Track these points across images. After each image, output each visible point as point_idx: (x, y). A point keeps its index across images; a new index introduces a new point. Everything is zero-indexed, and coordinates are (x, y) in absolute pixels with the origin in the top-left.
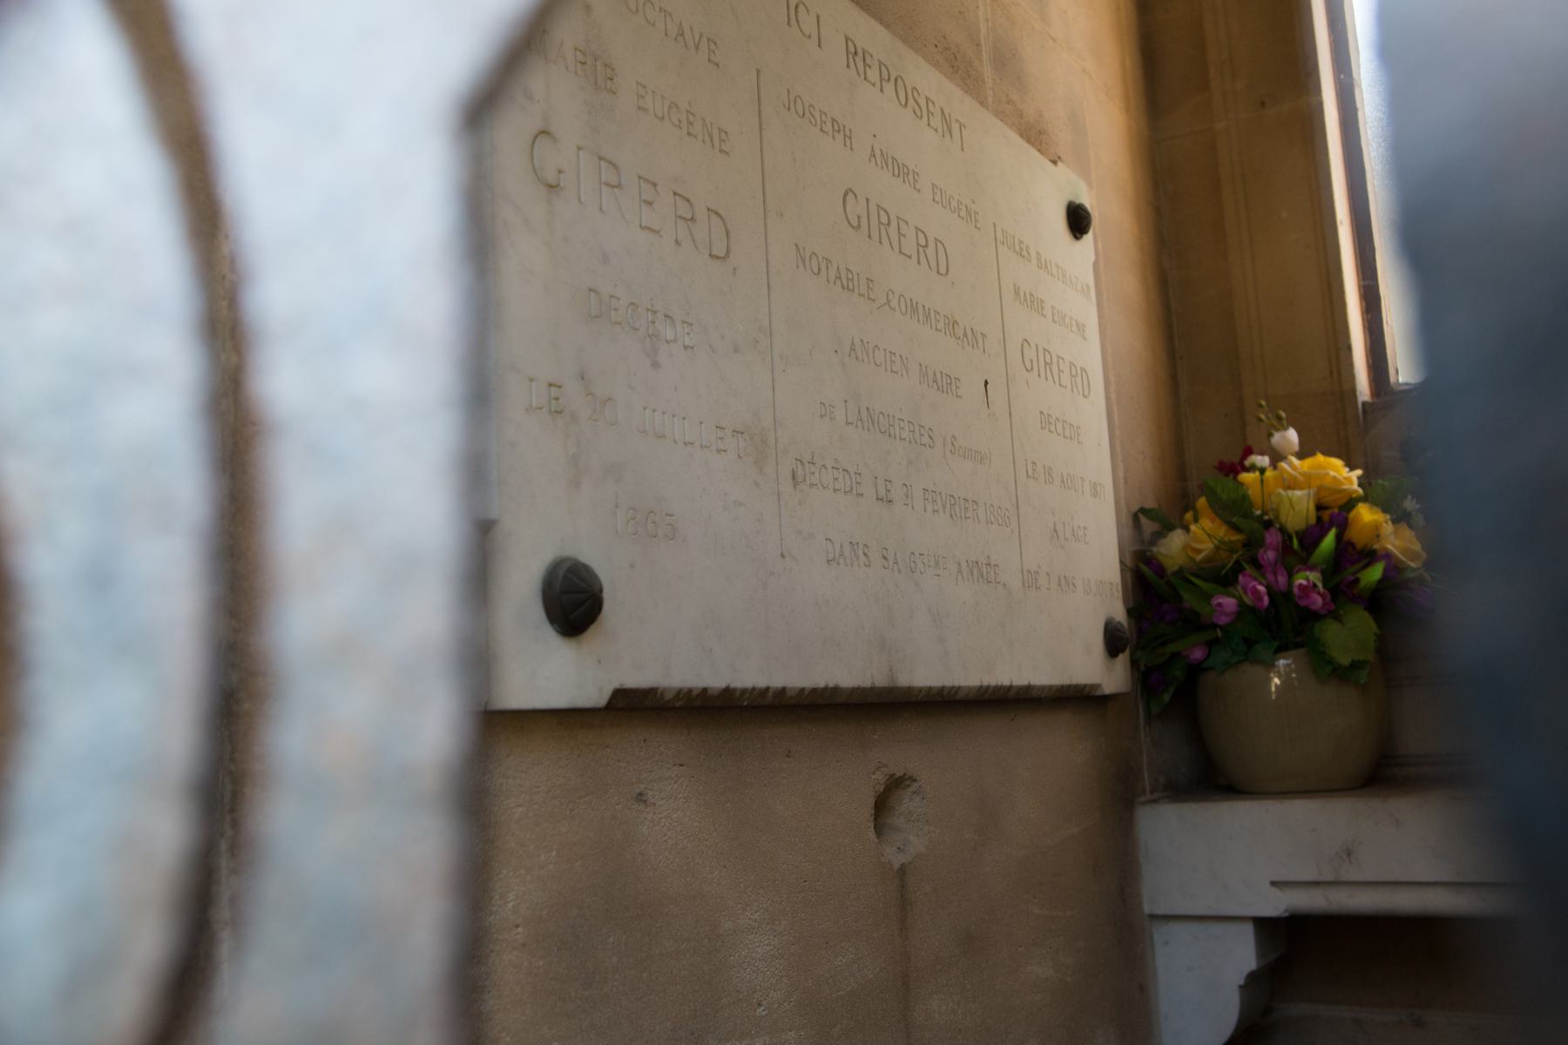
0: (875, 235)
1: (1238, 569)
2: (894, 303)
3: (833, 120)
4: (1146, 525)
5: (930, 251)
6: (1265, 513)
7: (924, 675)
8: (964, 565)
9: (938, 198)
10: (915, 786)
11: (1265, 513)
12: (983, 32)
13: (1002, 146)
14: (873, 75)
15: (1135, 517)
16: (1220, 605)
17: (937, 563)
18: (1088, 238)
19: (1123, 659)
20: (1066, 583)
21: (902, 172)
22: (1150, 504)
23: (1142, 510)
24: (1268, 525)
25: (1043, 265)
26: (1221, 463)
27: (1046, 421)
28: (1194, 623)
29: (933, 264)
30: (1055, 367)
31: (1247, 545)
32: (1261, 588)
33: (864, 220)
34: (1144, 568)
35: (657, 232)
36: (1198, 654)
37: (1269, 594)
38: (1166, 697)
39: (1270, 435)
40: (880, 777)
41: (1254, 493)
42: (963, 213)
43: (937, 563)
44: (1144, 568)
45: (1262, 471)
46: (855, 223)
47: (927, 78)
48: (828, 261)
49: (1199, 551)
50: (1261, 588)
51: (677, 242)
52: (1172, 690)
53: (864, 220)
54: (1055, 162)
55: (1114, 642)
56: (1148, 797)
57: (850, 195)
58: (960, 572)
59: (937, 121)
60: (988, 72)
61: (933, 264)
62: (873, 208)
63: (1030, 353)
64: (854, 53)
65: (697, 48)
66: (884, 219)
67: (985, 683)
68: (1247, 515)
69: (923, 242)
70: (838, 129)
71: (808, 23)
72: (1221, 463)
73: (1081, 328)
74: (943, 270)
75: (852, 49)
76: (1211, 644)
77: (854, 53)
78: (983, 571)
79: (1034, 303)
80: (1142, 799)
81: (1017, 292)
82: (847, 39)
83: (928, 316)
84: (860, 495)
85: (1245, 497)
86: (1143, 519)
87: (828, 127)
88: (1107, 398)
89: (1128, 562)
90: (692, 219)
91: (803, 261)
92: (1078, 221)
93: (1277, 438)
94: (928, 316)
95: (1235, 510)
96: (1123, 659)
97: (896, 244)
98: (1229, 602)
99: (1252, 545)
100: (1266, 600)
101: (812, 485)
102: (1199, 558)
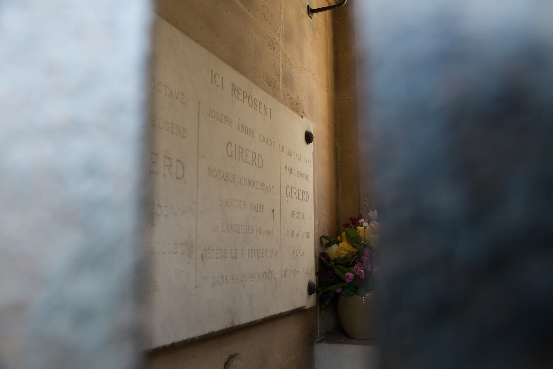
0: (237, 156)
1: (354, 263)
2: (242, 182)
3: (225, 117)
4: (325, 242)
5: (257, 160)
6: (365, 242)
7: (244, 320)
8: (261, 274)
9: (261, 139)
10: (238, 357)
11: (365, 242)
12: (281, 70)
13: (284, 114)
14: (241, 97)
15: (321, 239)
16: (348, 276)
17: (251, 276)
18: (312, 144)
19: (313, 296)
20: (296, 272)
21: (249, 131)
22: (326, 234)
23: (323, 236)
24: (366, 246)
25: (296, 156)
26: (351, 218)
27: (293, 214)
28: (340, 280)
29: (257, 165)
30: (297, 193)
31: (358, 253)
32: (362, 271)
33: (234, 153)
34: (322, 258)
35: (199, 103)
36: (339, 291)
37: (365, 273)
38: (327, 303)
39: (369, 212)
40: (227, 357)
41: (362, 234)
42: (269, 143)
43: (251, 276)
44: (322, 258)
45: (365, 228)
46: (230, 154)
47: (259, 94)
48: (220, 171)
49: (342, 254)
50: (362, 271)
51: (165, 176)
52: (329, 300)
53: (234, 153)
54: (302, 117)
55: (311, 290)
56: (319, 339)
57: (230, 144)
58: (259, 277)
59: (262, 110)
60: (281, 85)
61: (257, 165)
62: (237, 148)
63: (289, 190)
64: (235, 90)
65: (177, 98)
66: (241, 151)
67: (266, 316)
68: (358, 243)
69: (254, 157)
70: (228, 121)
71: (219, 81)
72: (351, 218)
73: (307, 177)
74: (260, 166)
75: (234, 88)
76: (343, 288)
77: (235, 90)
78: (267, 275)
79: (291, 171)
80: (317, 340)
81: (286, 168)
82: (232, 84)
83: (254, 184)
84: (225, 257)
85: (359, 236)
86: (323, 239)
87: (223, 120)
88: (315, 225)
89: (317, 256)
90: (171, 165)
91: (211, 173)
92: (309, 138)
93: (370, 214)
94: (254, 184)
95: (354, 241)
96: (313, 296)
97: (244, 159)
98: (351, 275)
99: (359, 254)
100: (364, 275)
101: (208, 258)
102: (342, 256)
